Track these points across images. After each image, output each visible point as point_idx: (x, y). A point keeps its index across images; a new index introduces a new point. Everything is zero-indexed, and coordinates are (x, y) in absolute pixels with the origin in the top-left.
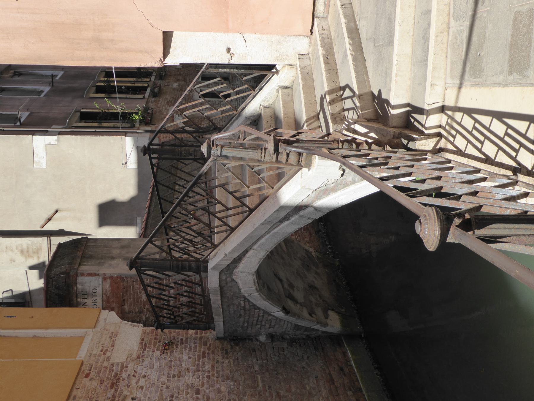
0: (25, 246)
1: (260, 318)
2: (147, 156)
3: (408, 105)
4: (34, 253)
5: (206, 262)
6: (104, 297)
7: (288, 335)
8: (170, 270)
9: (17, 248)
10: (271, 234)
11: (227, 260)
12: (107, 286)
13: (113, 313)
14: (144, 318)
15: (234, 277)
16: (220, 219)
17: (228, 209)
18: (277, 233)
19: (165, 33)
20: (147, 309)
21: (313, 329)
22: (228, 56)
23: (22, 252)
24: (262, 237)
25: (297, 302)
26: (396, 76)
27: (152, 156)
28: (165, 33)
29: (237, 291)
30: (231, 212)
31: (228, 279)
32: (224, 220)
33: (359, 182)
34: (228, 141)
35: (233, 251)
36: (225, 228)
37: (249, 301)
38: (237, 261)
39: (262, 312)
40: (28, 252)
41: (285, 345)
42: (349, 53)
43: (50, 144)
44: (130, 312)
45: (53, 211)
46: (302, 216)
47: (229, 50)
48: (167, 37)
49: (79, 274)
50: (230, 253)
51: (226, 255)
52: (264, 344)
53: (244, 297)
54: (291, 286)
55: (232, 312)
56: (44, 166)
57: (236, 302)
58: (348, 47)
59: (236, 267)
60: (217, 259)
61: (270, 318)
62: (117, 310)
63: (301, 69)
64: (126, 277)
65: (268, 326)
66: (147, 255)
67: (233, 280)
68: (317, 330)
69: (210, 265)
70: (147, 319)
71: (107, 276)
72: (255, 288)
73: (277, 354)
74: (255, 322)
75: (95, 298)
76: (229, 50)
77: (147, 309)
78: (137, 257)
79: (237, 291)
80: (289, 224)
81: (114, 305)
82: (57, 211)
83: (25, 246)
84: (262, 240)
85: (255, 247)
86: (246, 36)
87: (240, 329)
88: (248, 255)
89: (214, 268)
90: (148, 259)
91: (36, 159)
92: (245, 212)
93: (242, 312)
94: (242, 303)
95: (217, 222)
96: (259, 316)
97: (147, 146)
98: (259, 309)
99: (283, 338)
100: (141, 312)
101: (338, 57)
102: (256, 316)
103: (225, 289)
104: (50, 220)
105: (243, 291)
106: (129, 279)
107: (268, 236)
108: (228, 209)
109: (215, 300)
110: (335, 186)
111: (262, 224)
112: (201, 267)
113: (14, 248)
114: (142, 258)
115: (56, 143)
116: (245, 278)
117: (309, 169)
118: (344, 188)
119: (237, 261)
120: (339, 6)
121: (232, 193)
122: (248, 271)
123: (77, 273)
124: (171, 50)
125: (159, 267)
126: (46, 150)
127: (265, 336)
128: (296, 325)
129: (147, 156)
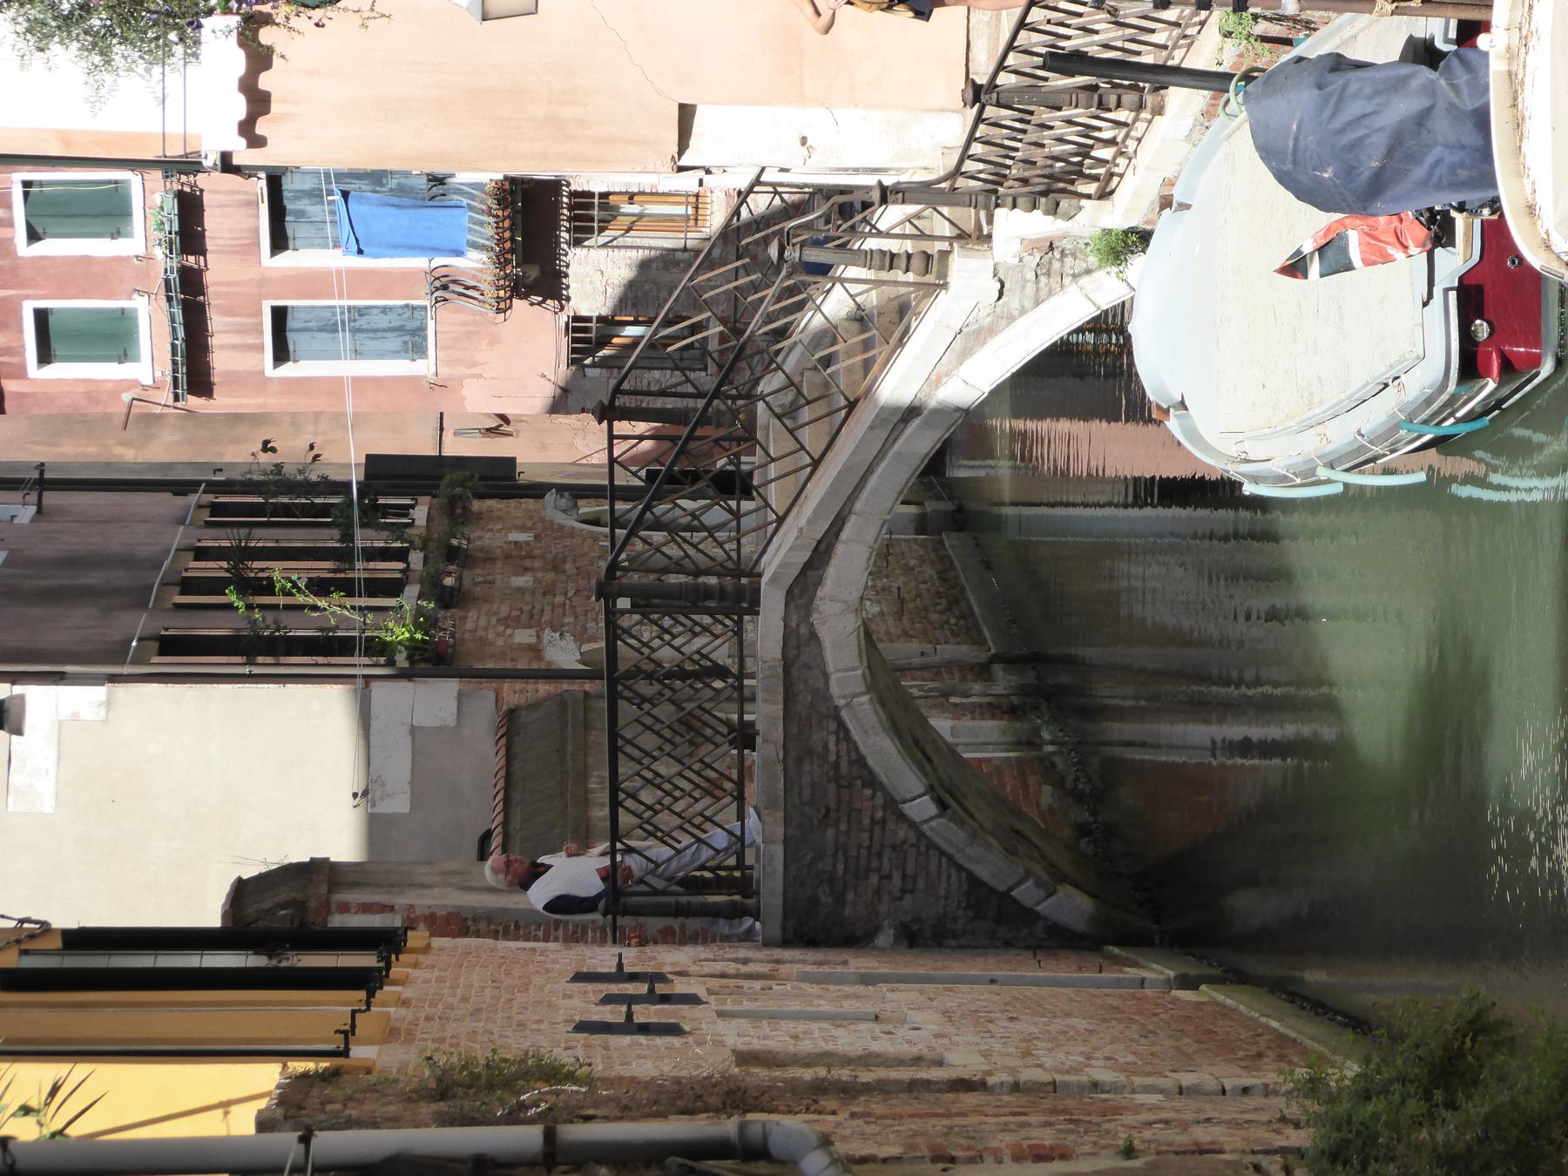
3: (1112, 192)
19: (682, 107)
28: (682, 107)
29: (821, 684)
34: (766, 713)
43: (75, 717)
47: (804, 141)
48: (686, 114)
49: (333, 906)
51: (801, 530)
56: (48, 806)
59: (819, 582)
64: (474, 920)
71: (418, 913)
72: (860, 672)
76: (804, 141)
84: (872, 482)
85: (858, 506)
91: (15, 778)
97: (606, 402)
107: (883, 464)
111: (871, 428)
115: (102, 713)
123: (328, 902)
124: (692, 142)
126: (59, 743)
127: (891, 932)
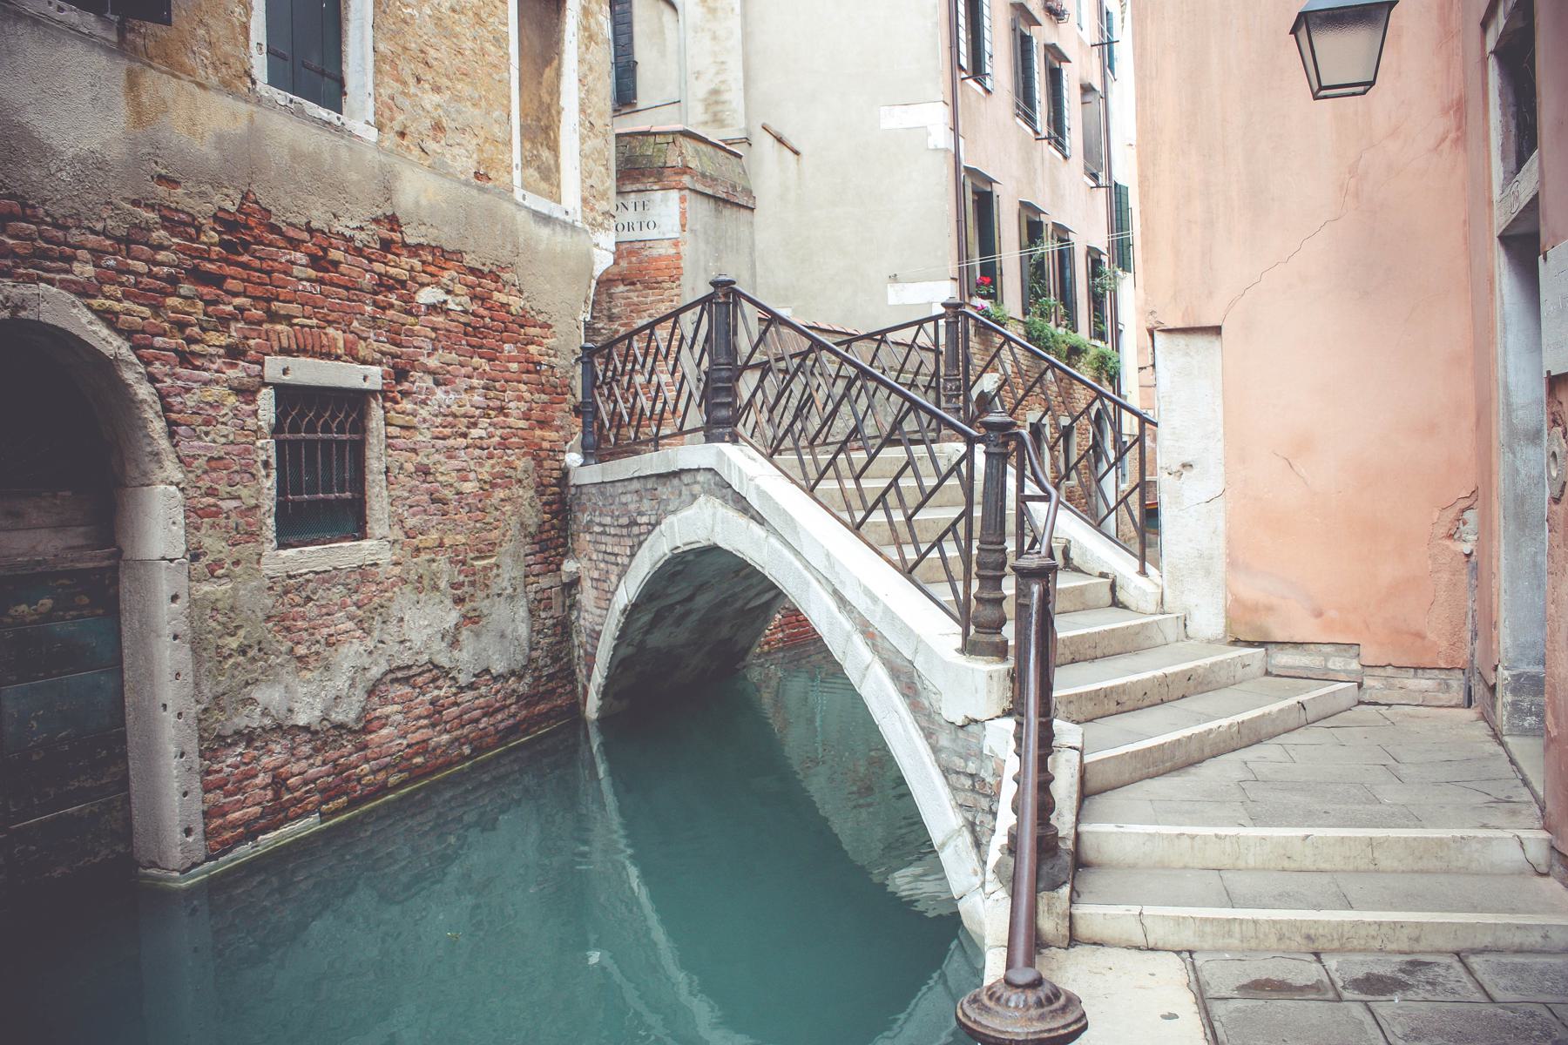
0: (726, 97)
1: (613, 558)
2: (943, 310)
4: (715, 114)
5: (735, 439)
6: (638, 245)
7: (578, 618)
8: (711, 361)
9: (723, 82)
10: (805, 573)
11: (741, 482)
12: (665, 250)
13: (610, 260)
14: (600, 325)
15: (702, 499)
16: (832, 462)
17: (857, 478)
18: (808, 584)
20: (617, 331)
21: (590, 669)
22: (1175, 467)
23: (715, 92)
24: (797, 553)
25: (647, 632)
26: (1193, 837)
27: (942, 322)
29: (671, 508)
30: (850, 484)
31: (697, 489)
32: (831, 471)
33: (937, 761)
35: (762, 494)
36: (813, 475)
37: (649, 532)
38: (741, 504)
39: (626, 560)
40: (717, 103)
41: (557, 612)
42: (1213, 725)
44: (611, 296)
45: (797, 147)
46: (849, 638)
50: (757, 487)
52: (559, 569)
53: (658, 523)
54: (679, 622)
55: (624, 499)
57: (646, 505)
58: (1225, 722)
60: (742, 462)
61: (614, 578)
62: (616, 270)
63: (1156, 622)
65: (596, 575)
66: (744, 317)
67: (694, 497)
68: (589, 678)
69: (727, 448)
70: (597, 332)
73: (539, 596)
74: (603, 548)
75: (637, 226)
77: (617, 331)
78: (739, 295)
79: (671, 508)
80: (828, 610)
81: (624, 264)
82: (797, 153)
83: (726, 97)
86: (1220, 503)
87: (586, 518)
88: (754, 526)
89: (721, 454)
90: (735, 318)
92: (852, 516)
93: (624, 521)
94: (644, 519)
95: (824, 458)
96: (616, 555)
98: (633, 555)
99: (571, 607)
100: (611, 318)
101: (1195, 704)
102: (616, 550)
103: (676, 482)
104: (780, 140)
105: (671, 519)
106: (676, 291)
108: (857, 478)
109: (650, 462)
110: (923, 708)
112: (721, 426)
113: (721, 78)
114: (736, 304)
116: (695, 524)
117: (962, 651)
118: (922, 729)
119: (741, 504)
120: (1301, 698)
121: (894, 482)
122: (717, 529)
125: (721, 340)
128: (599, 633)
129: (943, 310)
